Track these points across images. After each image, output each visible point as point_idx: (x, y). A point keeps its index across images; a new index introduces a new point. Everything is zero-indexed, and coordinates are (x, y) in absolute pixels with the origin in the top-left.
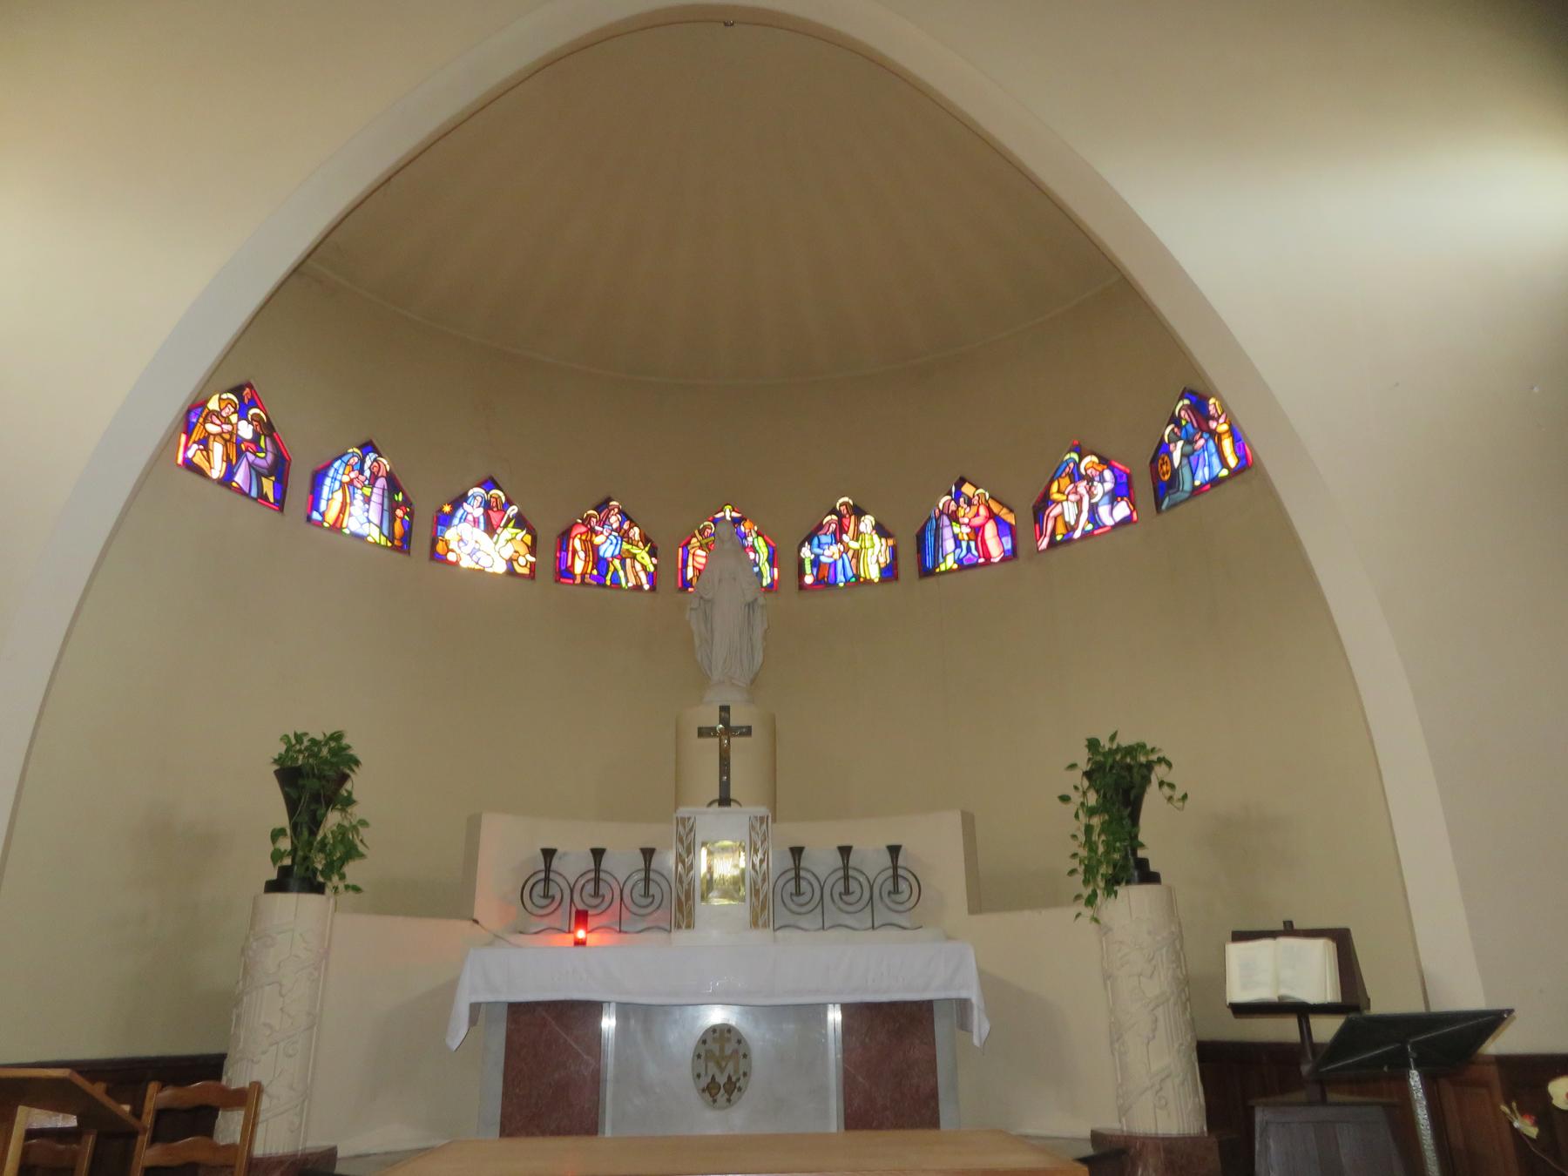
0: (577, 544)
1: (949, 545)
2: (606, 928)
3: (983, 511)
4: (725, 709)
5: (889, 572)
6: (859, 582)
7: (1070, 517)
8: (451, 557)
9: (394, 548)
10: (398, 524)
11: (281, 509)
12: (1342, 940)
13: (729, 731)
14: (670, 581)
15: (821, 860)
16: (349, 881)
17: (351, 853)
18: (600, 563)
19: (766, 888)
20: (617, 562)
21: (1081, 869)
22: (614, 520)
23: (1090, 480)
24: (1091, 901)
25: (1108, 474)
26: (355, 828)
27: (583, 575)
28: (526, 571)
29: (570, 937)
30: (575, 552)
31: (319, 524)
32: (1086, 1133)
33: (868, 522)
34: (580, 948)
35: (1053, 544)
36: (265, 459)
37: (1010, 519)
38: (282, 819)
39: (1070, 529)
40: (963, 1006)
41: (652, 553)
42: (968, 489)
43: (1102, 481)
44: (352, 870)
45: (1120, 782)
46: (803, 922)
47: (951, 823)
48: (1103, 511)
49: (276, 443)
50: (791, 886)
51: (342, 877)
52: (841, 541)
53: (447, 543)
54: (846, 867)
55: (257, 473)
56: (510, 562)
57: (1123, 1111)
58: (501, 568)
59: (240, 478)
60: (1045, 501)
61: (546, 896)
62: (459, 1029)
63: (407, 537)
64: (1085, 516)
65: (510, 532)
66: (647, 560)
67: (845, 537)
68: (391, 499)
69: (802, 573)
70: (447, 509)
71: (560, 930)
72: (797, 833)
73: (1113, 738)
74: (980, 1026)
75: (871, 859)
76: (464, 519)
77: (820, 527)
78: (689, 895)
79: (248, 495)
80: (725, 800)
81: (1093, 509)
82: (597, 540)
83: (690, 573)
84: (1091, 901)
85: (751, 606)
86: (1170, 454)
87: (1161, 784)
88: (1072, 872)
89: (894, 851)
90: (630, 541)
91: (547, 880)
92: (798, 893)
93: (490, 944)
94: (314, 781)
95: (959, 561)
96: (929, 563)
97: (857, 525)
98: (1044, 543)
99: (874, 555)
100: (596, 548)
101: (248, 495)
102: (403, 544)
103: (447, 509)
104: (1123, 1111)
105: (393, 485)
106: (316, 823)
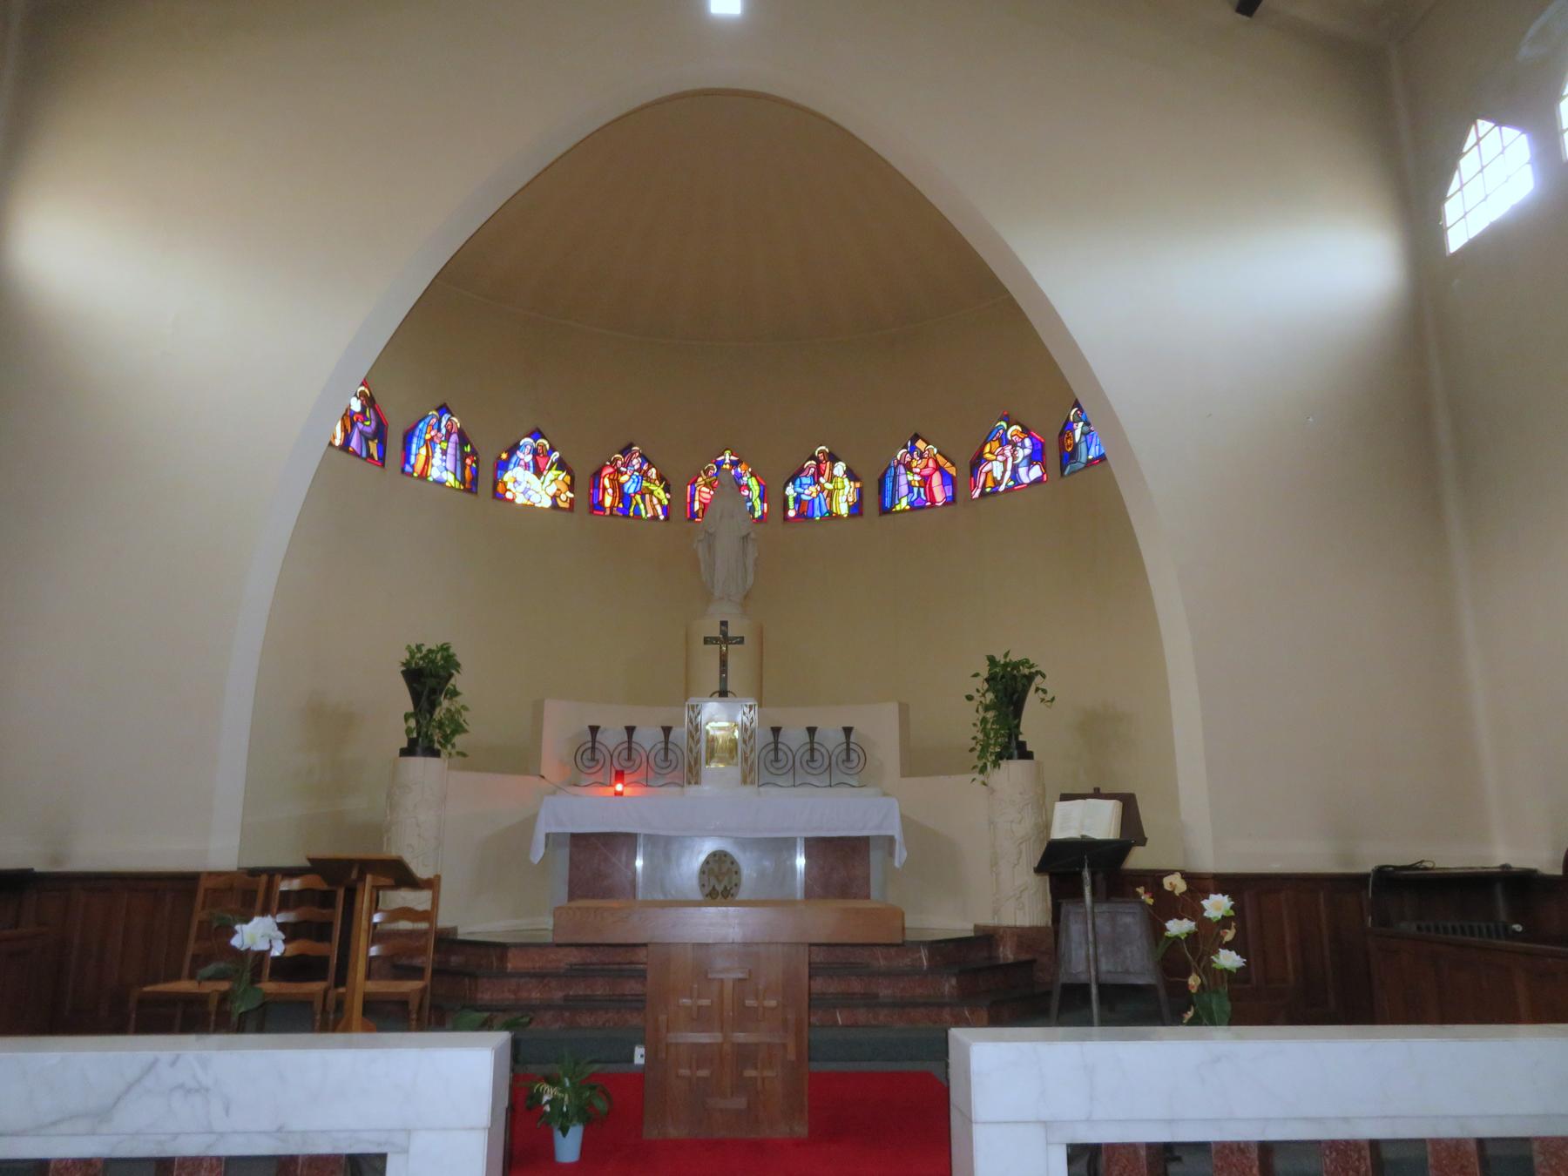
0: (607, 482)
1: (904, 489)
2: (636, 783)
3: (931, 464)
4: (724, 624)
5: (856, 509)
6: (832, 516)
7: (997, 474)
8: (509, 495)
9: (465, 490)
10: (468, 471)
11: (383, 465)
12: (1129, 805)
13: (724, 634)
14: (680, 512)
15: (794, 738)
16: (458, 748)
17: (459, 729)
18: (625, 498)
19: (753, 757)
20: (638, 497)
21: (979, 748)
22: (636, 462)
23: (1014, 445)
24: (983, 770)
25: (1027, 442)
26: (459, 712)
27: (611, 507)
28: (566, 505)
29: (611, 790)
30: (605, 489)
31: (410, 475)
32: (971, 926)
33: (840, 468)
34: (619, 798)
35: (983, 494)
36: (369, 425)
37: (952, 471)
38: (410, 708)
39: (997, 483)
40: (891, 840)
41: (666, 490)
42: (920, 444)
43: (1023, 447)
44: (457, 739)
45: (1010, 688)
46: (780, 781)
47: (890, 711)
48: (1022, 471)
49: (378, 414)
50: (772, 756)
51: (453, 746)
52: (818, 482)
53: (505, 484)
54: (812, 742)
55: (366, 438)
56: (554, 498)
57: (996, 912)
58: (547, 503)
59: (354, 443)
60: (978, 460)
61: (593, 759)
62: (538, 853)
63: (475, 480)
64: (1008, 474)
65: (552, 474)
66: (662, 495)
67: (822, 480)
68: (462, 451)
69: (786, 508)
70: (504, 456)
71: (602, 784)
72: (778, 716)
73: (1006, 655)
74: (900, 855)
75: (831, 738)
76: (517, 464)
77: (802, 470)
78: (697, 761)
79: (359, 456)
80: (723, 693)
81: (1015, 468)
82: (623, 479)
83: (697, 506)
84: (983, 770)
85: (745, 538)
86: (1073, 431)
87: (1037, 690)
88: (972, 750)
89: (848, 731)
90: (649, 480)
91: (593, 748)
92: (777, 760)
93: (554, 793)
94: (428, 679)
95: (910, 503)
96: (888, 504)
97: (832, 470)
98: (977, 494)
99: (844, 496)
100: (621, 486)
101: (359, 456)
102: (470, 485)
103: (504, 456)
104: (996, 912)
105: (463, 440)
106: (433, 705)
